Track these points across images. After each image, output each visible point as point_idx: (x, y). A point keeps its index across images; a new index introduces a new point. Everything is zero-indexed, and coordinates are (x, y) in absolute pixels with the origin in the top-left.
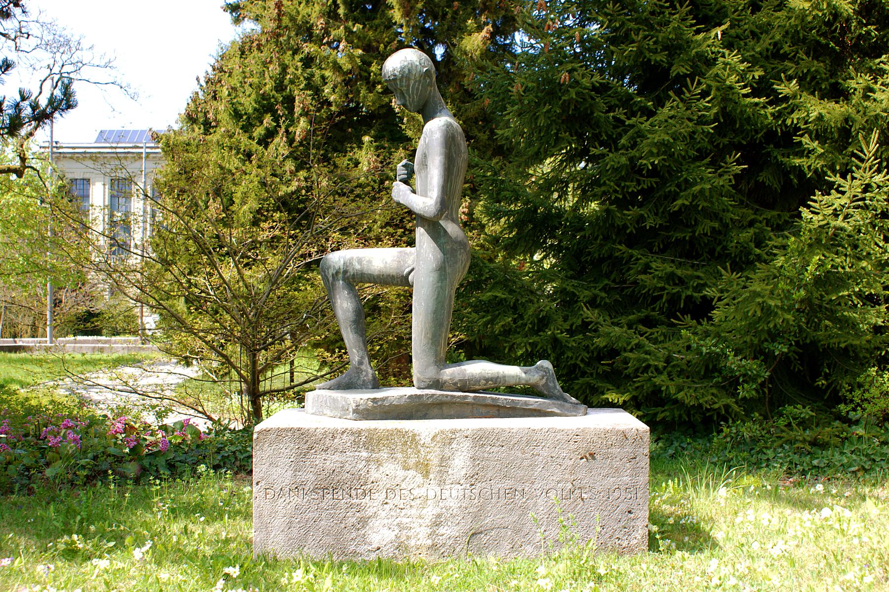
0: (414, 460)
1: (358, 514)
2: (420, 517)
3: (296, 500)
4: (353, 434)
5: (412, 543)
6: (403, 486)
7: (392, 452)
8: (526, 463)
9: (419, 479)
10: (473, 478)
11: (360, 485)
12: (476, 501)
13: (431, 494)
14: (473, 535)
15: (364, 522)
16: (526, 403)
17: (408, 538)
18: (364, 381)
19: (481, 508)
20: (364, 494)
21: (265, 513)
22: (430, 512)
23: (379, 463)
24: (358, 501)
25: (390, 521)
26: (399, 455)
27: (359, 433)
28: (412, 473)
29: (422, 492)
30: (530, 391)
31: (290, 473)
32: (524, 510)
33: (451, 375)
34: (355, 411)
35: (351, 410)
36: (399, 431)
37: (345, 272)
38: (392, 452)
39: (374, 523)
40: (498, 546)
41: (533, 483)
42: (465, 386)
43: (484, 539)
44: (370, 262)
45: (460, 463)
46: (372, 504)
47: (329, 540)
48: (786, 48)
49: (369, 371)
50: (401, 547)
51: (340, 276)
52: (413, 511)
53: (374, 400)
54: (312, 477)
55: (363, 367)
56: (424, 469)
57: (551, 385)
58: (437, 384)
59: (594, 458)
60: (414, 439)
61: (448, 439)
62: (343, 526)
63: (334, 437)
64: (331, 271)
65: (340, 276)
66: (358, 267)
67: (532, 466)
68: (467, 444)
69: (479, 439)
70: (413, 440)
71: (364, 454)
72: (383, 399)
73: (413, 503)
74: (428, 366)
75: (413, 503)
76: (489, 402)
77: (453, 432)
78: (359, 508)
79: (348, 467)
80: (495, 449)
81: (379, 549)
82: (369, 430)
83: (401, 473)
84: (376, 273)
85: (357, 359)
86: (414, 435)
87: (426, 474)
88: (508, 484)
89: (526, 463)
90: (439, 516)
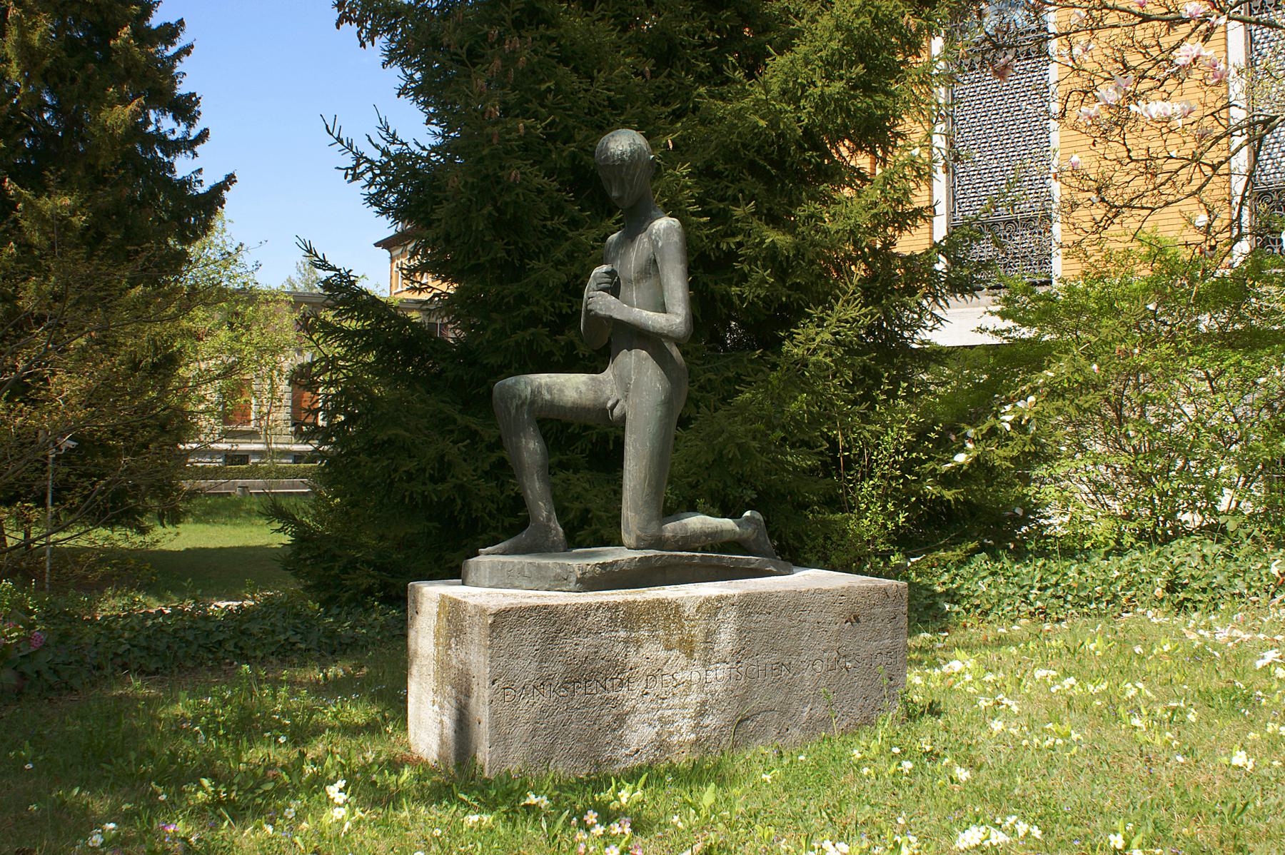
0: (677, 638)
1: (614, 711)
2: (684, 708)
3: (540, 700)
4: (609, 609)
5: (675, 739)
6: (665, 670)
7: (653, 629)
8: (793, 632)
9: (683, 661)
10: (739, 654)
11: (616, 672)
12: (742, 681)
13: (695, 677)
14: (741, 721)
15: (621, 719)
16: (748, 562)
17: (671, 734)
18: (554, 542)
19: (748, 689)
20: (621, 684)
21: (504, 720)
22: (694, 698)
23: (638, 644)
24: (613, 694)
25: (650, 716)
26: (661, 633)
27: (617, 606)
28: (676, 653)
29: (685, 676)
30: (735, 545)
31: (534, 665)
32: (791, 687)
33: (674, 531)
34: (578, 581)
35: (573, 579)
36: (660, 603)
37: (533, 402)
38: (653, 629)
39: (632, 720)
40: (765, 733)
41: (799, 655)
42: (687, 542)
43: (751, 725)
44: (561, 391)
45: (726, 638)
46: (631, 696)
47: (580, 747)
48: (720, 166)
49: (558, 531)
50: (662, 745)
51: (525, 407)
52: (676, 701)
53: (603, 566)
54: (560, 668)
55: (552, 525)
56: (687, 647)
57: (762, 539)
58: (658, 543)
59: (858, 621)
60: (677, 611)
61: (712, 608)
62: (596, 727)
63: (587, 615)
64: (516, 402)
65: (525, 407)
66: (547, 397)
67: (800, 634)
68: (733, 614)
69: (747, 605)
70: (673, 611)
71: (622, 634)
72: (612, 564)
73: (675, 691)
74: (649, 522)
75: (675, 691)
76: (715, 562)
77: (720, 599)
78: (617, 703)
79: (603, 652)
80: (762, 618)
81: (637, 751)
82: (627, 603)
83: (663, 654)
84: (569, 405)
85: (544, 514)
86: (678, 606)
87: (690, 655)
88: (775, 657)
89: (793, 632)
90: (704, 703)
